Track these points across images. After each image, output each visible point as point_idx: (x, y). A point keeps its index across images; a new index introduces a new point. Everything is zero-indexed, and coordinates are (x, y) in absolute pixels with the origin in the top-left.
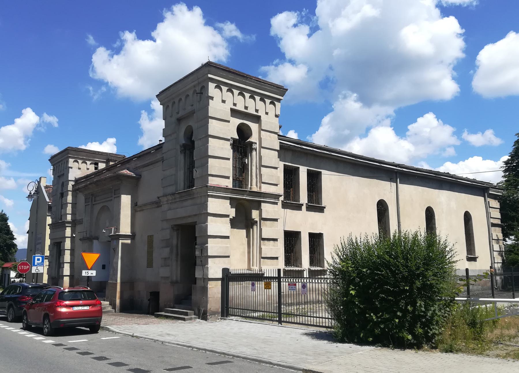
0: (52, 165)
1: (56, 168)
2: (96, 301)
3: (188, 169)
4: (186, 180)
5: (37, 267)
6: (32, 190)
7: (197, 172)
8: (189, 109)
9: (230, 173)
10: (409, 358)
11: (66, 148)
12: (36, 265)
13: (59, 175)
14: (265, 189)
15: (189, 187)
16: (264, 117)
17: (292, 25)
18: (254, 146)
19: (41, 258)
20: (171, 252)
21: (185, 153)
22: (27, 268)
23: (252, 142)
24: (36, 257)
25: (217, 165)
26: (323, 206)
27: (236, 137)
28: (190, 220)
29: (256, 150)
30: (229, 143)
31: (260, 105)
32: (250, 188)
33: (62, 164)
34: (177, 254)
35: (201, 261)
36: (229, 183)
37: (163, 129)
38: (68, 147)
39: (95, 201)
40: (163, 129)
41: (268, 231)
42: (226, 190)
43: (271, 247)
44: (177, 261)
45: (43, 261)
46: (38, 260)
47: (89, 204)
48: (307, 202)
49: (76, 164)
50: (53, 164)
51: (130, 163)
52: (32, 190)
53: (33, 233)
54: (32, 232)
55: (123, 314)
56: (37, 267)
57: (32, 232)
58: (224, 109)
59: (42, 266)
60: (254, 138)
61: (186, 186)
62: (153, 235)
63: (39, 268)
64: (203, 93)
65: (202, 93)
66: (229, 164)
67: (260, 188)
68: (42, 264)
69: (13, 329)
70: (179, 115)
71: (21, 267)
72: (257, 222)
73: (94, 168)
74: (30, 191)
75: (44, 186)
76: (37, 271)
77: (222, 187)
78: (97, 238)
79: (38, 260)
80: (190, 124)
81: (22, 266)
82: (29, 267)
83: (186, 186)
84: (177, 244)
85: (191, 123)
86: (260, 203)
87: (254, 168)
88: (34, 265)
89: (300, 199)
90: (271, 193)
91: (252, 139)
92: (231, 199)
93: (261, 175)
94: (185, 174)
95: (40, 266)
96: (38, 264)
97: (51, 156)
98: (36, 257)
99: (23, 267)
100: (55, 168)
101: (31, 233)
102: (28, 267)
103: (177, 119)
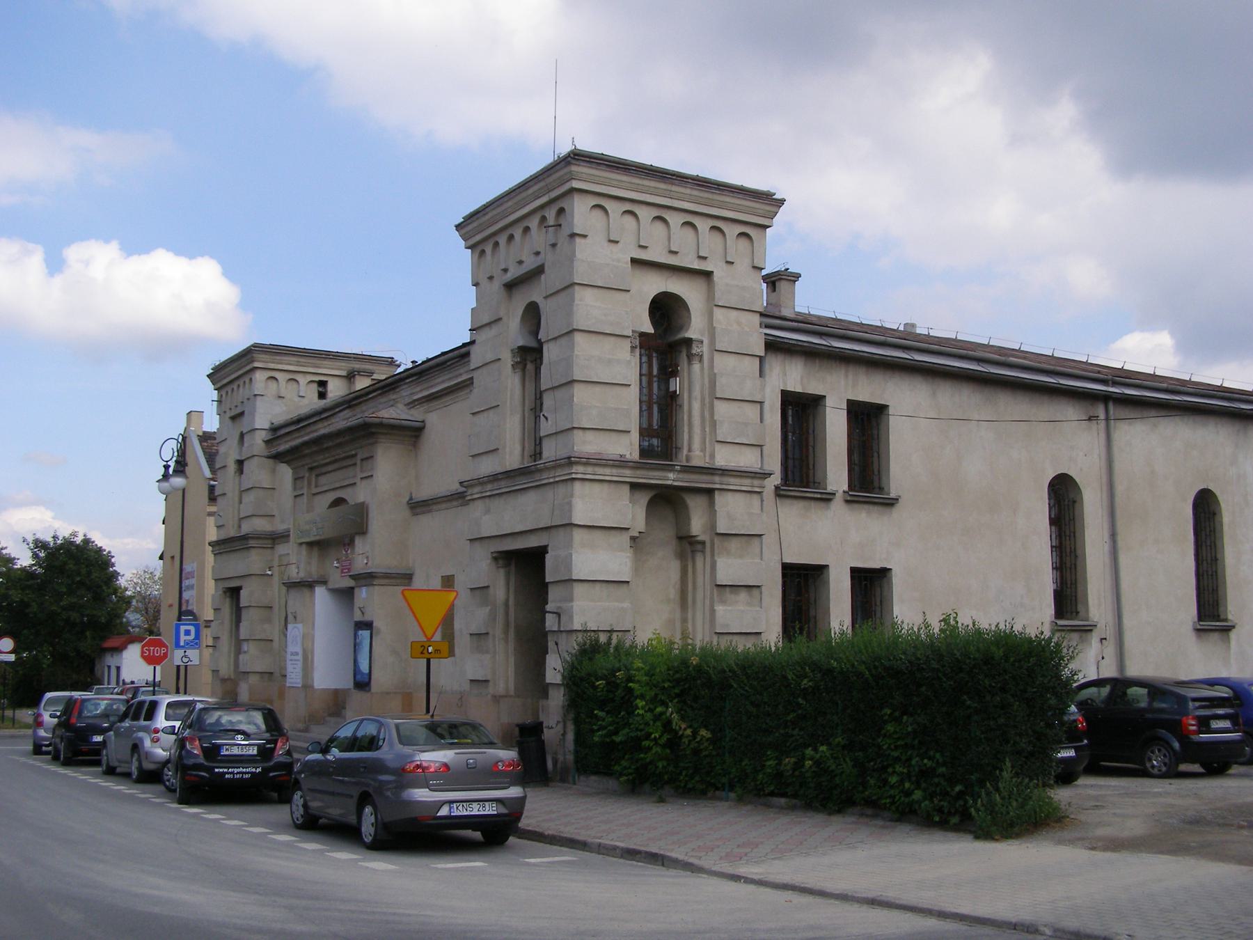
0: (215, 390)
1: (224, 396)
2: (1050, 934)
3: (531, 410)
4: (526, 438)
5: (185, 652)
6: (171, 459)
7: (549, 419)
8: (530, 263)
9: (632, 422)
10: (1223, 928)
11: (247, 348)
12: (182, 647)
13: (232, 414)
14: (724, 458)
15: (535, 455)
16: (720, 273)
17: (471, 352)
18: (695, 350)
19: (192, 628)
20: (493, 617)
21: (524, 369)
22: (163, 652)
23: (692, 339)
24: (181, 627)
25: (597, 405)
26: (892, 495)
27: (648, 328)
28: (533, 542)
29: (701, 357)
30: (627, 345)
31: (710, 243)
32: (687, 456)
33: (239, 386)
34: (507, 624)
35: (557, 644)
36: (628, 447)
37: (472, 309)
38: (253, 346)
39: (316, 486)
40: (472, 309)
41: (730, 567)
42: (621, 463)
43: (742, 608)
44: (506, 641)
45: (198, 636)
46: (187, 633)
47: (303, 494)
48: (846, 488)
49: (273, 385)
50: (219, 385)
51: (397, 390)
52: (171, 459)
53: (175, 559)
54: (173, 557)
55: (641, 846)
56: (185, 652)
57: (173, 557)
58: (615, 263)
59: (197, 649)
60: (695, 330)
61: (526, 453)
62: (454, 575)
63: (189, 652)
64: (562, 226)
65: (560, 225)
66: (631, 399)
67: (712, 456)
68: (196, 644)
69: (138, 792)
70: (509, 276)
71: (149, 651)
72: (703, 543)
73: (316, 395)
74: (167, 462)
75: (198, 436)
76: (185, 660)
77: (611, 457)
78: (323, 582)
79: (187, 633)
80: (533, 299)
81: (152, 648)
82: (167, 651)
83: (526, 453)
84: (507, 600)
85: (535, 294)
86: (710, 492)
87: (696, 406)
88: (178, 646)
89: (828, 481)
90: (742, 469)
91: (692, 333)
92: (634, 487)
93: (714, 424)
94: (524, 421)
95: (192, 647)
96: (188, 644)
97: (213, 366)
98: (181, 627)
99: (154, 650)
100: (222, 396)
101: (169, 558)
102: (163, 650)
103: (504, 285)
